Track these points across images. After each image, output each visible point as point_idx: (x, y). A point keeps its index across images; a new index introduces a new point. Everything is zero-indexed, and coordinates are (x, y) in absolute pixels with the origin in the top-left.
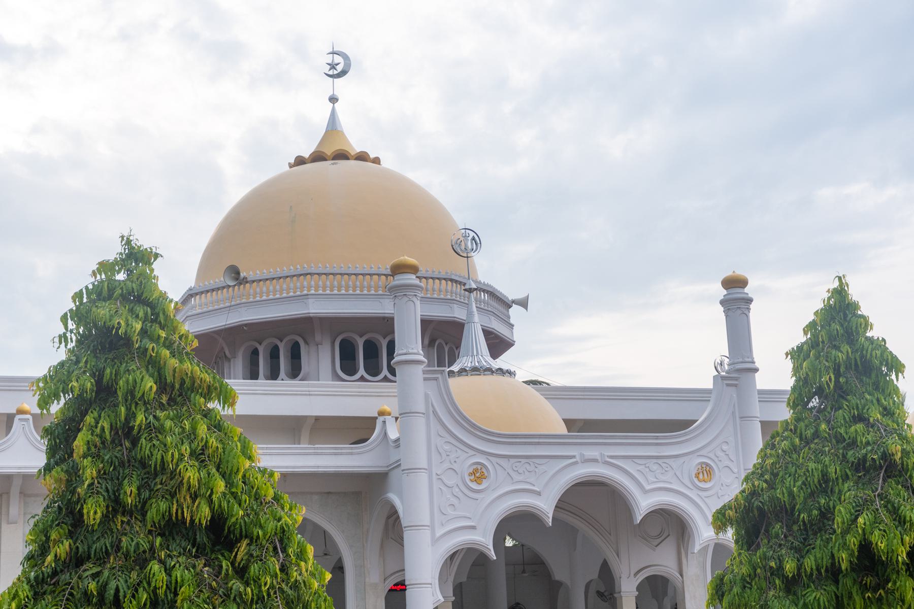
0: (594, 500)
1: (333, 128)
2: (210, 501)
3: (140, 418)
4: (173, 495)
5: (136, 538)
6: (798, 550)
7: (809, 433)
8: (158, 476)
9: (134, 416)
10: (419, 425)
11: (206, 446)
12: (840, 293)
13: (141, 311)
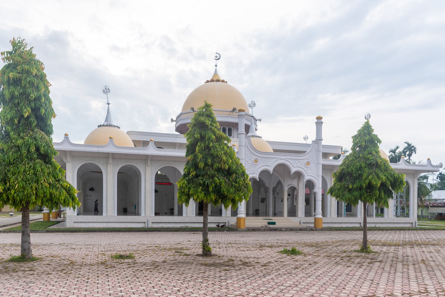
0: (282, 169)
1: (216, 73)
2: (228, 164)
3: (211, 144)
4: (219, 162)
5: (211, 172)
6: (352, 183)
7: (357, 156)
8: (215, 157)
9: (210, 144)
10: (243, 148)
11: (227, 152)
12: (367, 123)
13: (210, 119)
